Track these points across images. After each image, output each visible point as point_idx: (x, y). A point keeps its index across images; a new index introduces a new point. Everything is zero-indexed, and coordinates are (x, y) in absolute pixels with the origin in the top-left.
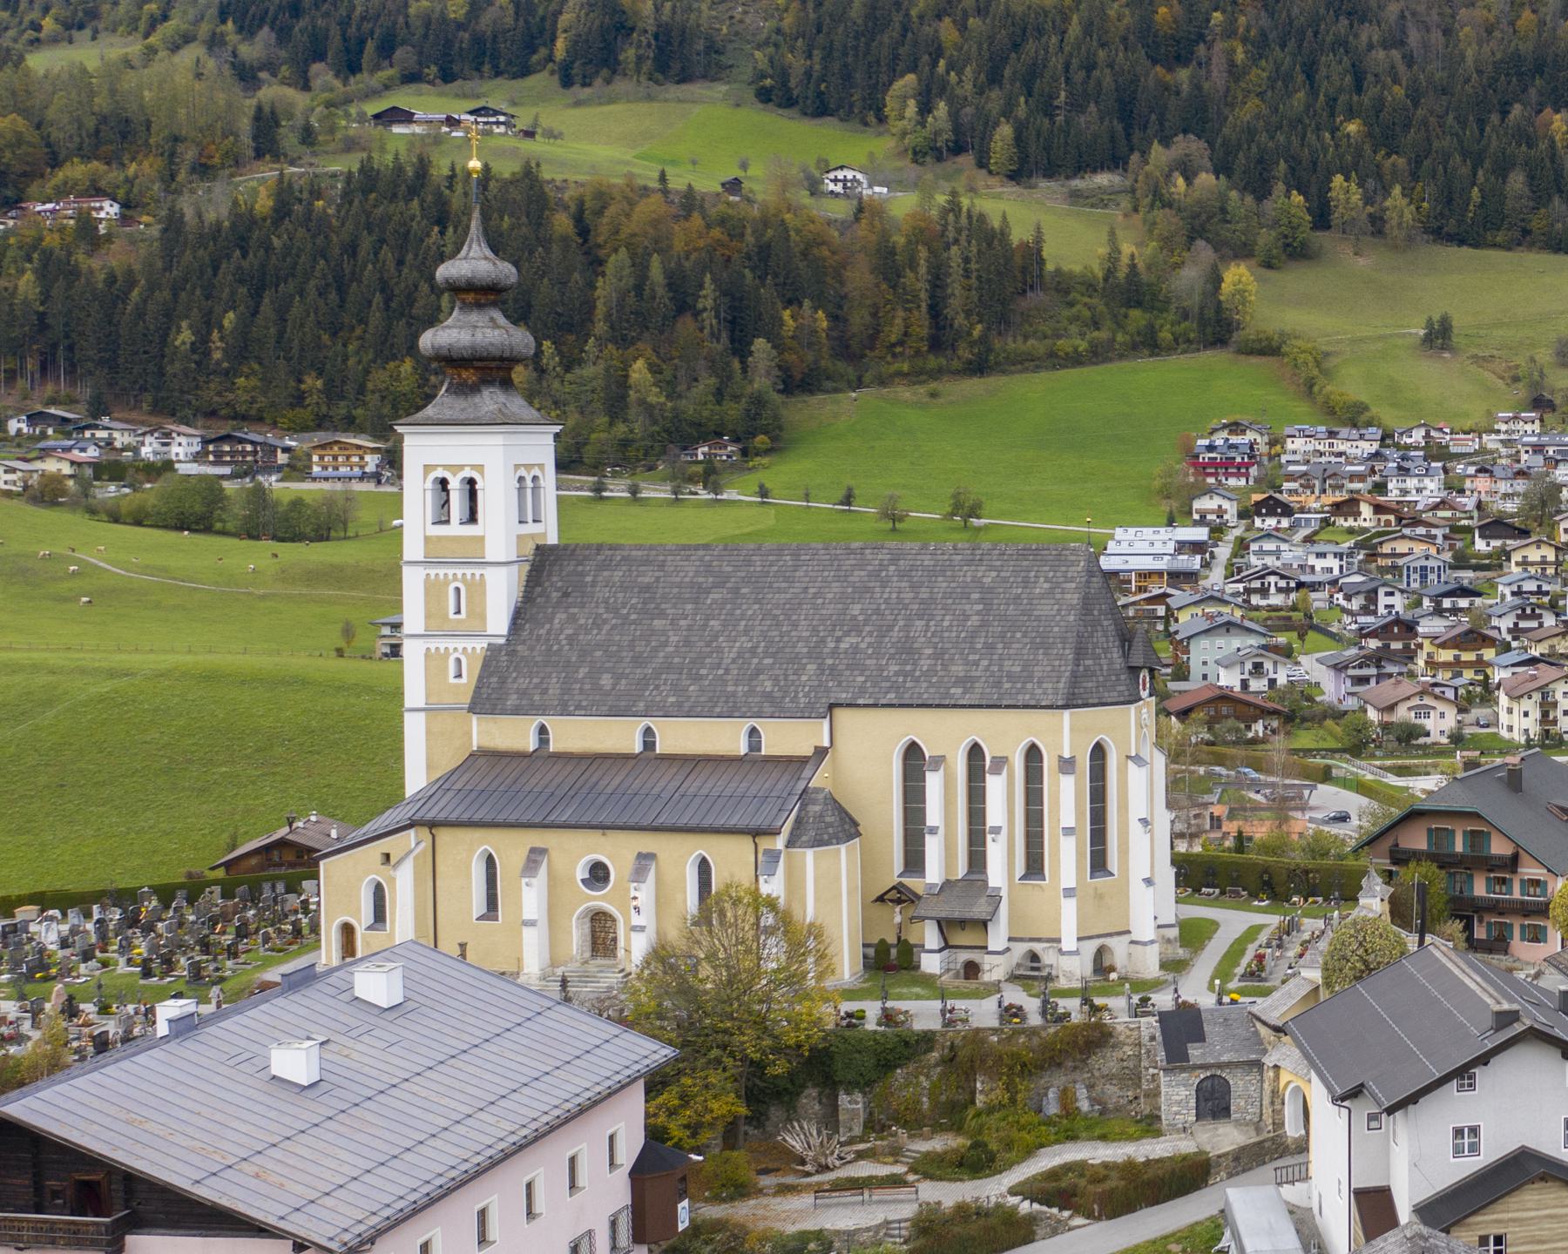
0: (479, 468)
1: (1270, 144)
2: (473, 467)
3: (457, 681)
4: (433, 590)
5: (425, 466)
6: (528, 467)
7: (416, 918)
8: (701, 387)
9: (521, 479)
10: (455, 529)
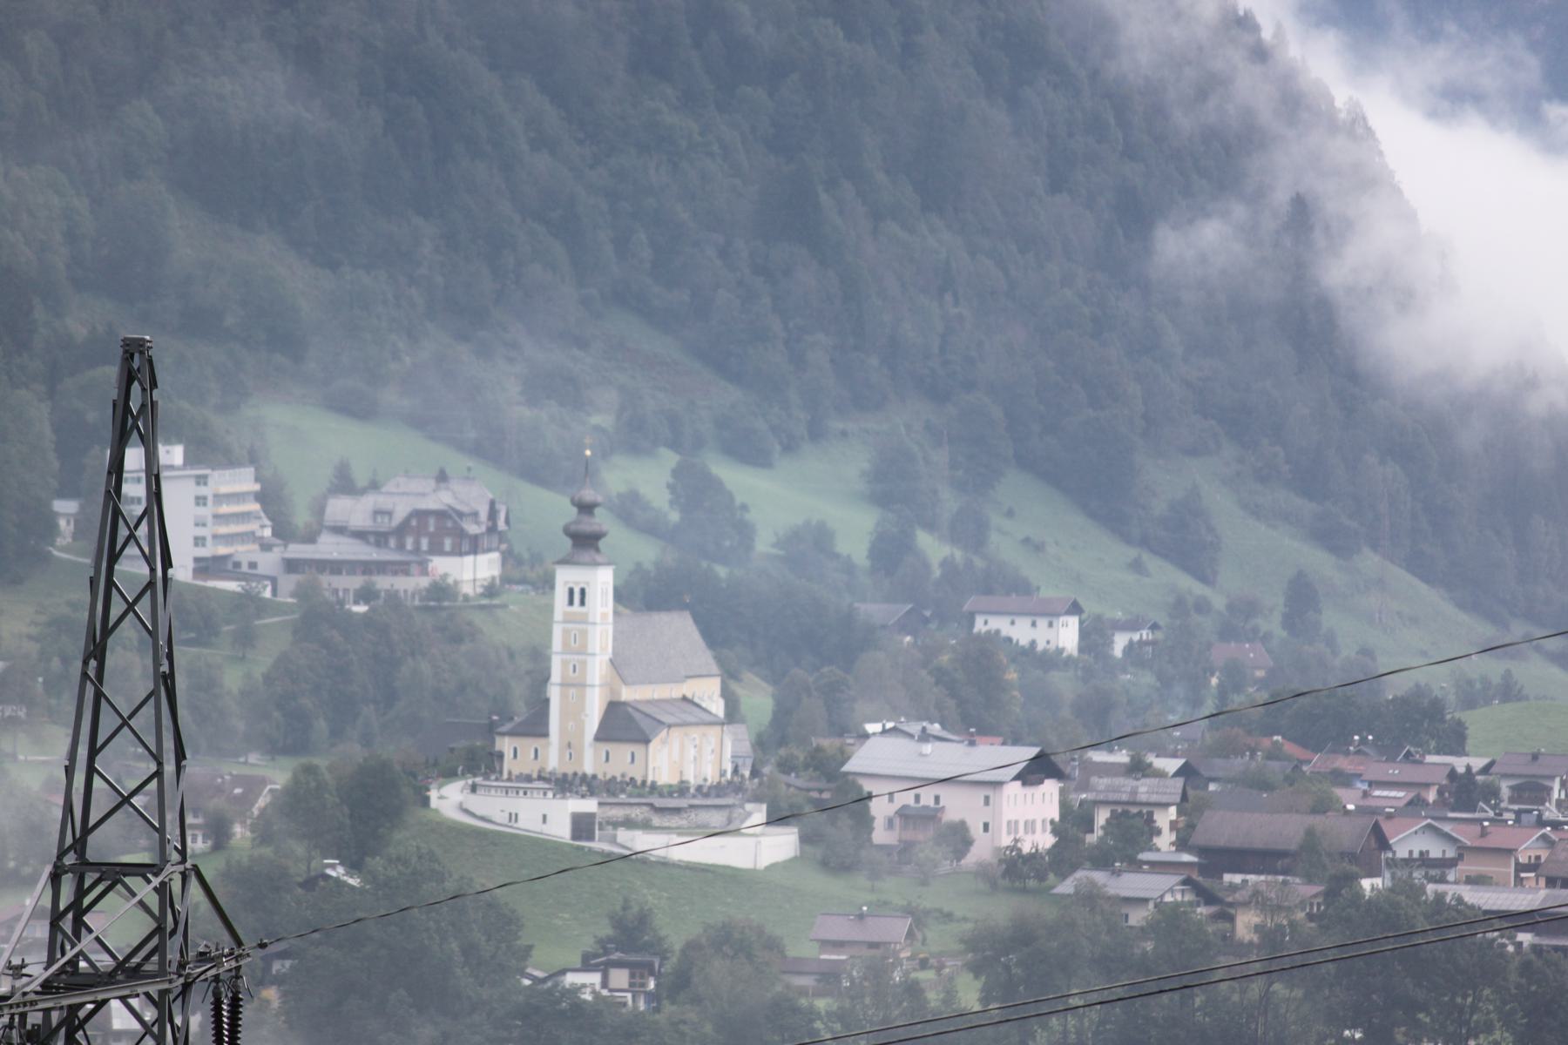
0: (588, 583)
4: (566, 632)
7: (148, 942)
8: (1084, 796)
10: (576, 607)
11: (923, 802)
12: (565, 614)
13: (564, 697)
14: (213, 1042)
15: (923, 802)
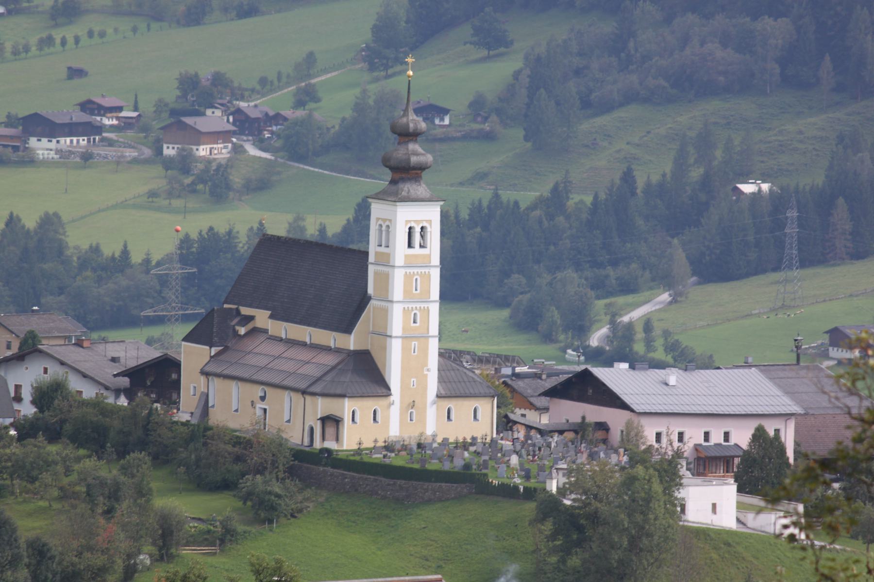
1: (652, 521)
2: (427, 221)
3: (415, 325)
4: (408, 277)
5: (431, 221)
6: (384, 220)
9: (381, 226)
11: (733, 441)
12: (406, 256)
13: (405, 350)
14: (12, 221)
15: (733, 441)
